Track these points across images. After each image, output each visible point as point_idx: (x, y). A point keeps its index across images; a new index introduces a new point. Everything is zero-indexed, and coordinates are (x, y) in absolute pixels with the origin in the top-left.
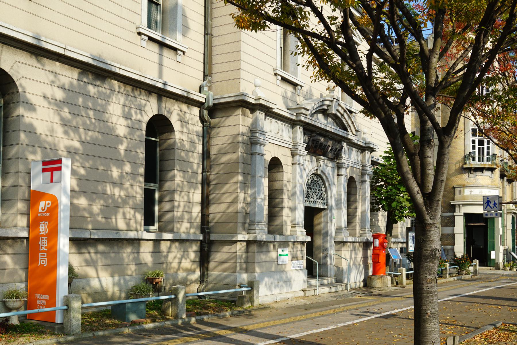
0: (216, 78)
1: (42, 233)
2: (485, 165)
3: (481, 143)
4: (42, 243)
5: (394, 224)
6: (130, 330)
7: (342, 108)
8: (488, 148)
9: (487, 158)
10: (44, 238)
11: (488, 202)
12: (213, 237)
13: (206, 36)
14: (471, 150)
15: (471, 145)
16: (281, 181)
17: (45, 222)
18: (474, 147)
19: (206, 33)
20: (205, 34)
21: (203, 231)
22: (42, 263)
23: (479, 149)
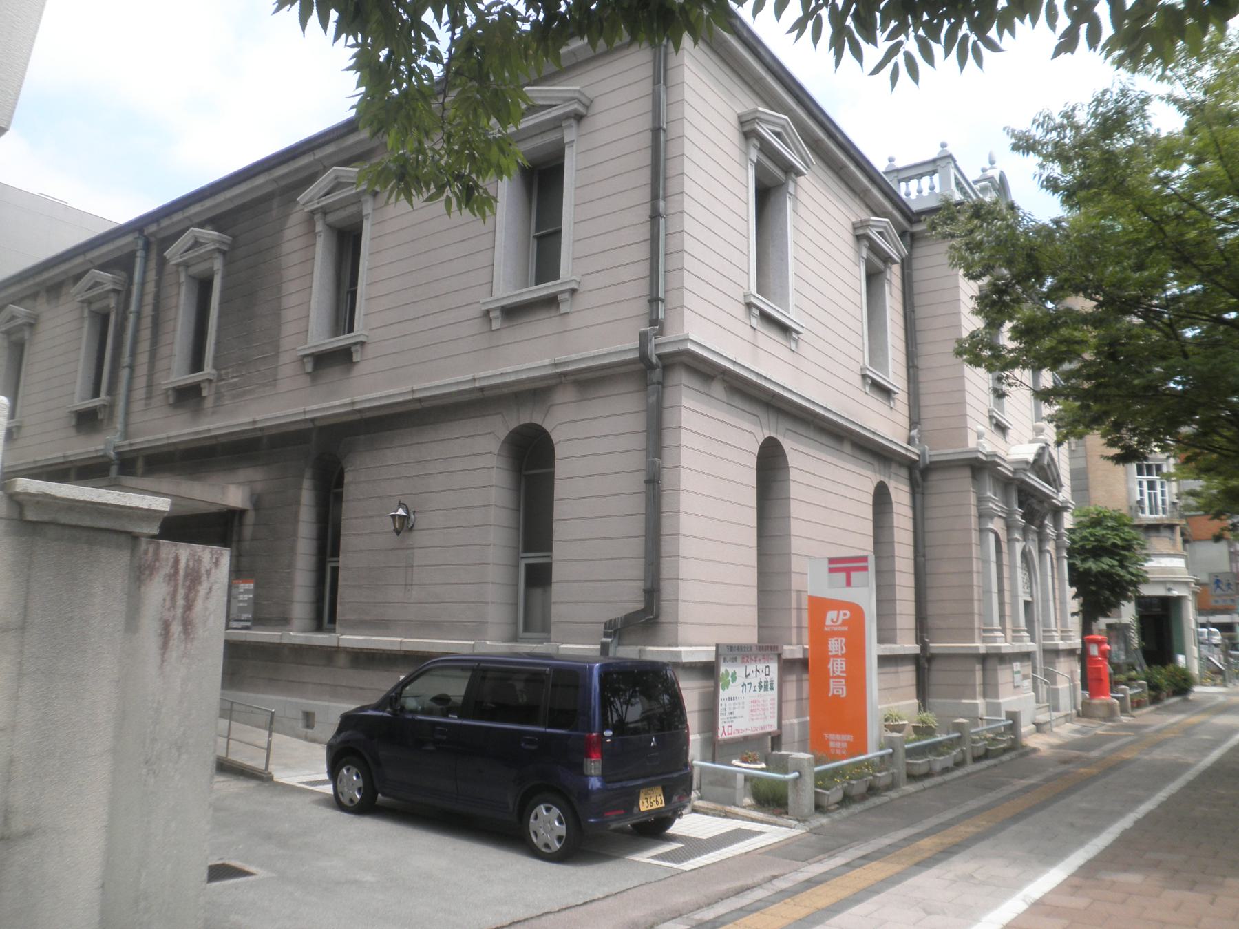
0: (926, 425)
1: (834, 653)
2: (1161, 519)
3: (1151, 485)
4: (835, 665)
5: (1094, 623)
6: (246, 597)
7: (983, 454)
8: (1163, 493)
9: (1163, 508)
10: (839, 660)
11: (1218, 582)
12: (936, 646)
13: (911, 370)
14: (1138, 498)
15: (1138, 488)
16: (674, 556)
17: (840, 639)
18: (1141, 493)
19: (911, 364)
20: (908, 368)
21: (920, 640)
22: (835, 693)
23: (1149, 494)
